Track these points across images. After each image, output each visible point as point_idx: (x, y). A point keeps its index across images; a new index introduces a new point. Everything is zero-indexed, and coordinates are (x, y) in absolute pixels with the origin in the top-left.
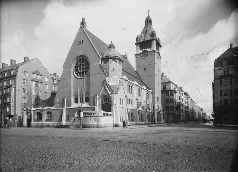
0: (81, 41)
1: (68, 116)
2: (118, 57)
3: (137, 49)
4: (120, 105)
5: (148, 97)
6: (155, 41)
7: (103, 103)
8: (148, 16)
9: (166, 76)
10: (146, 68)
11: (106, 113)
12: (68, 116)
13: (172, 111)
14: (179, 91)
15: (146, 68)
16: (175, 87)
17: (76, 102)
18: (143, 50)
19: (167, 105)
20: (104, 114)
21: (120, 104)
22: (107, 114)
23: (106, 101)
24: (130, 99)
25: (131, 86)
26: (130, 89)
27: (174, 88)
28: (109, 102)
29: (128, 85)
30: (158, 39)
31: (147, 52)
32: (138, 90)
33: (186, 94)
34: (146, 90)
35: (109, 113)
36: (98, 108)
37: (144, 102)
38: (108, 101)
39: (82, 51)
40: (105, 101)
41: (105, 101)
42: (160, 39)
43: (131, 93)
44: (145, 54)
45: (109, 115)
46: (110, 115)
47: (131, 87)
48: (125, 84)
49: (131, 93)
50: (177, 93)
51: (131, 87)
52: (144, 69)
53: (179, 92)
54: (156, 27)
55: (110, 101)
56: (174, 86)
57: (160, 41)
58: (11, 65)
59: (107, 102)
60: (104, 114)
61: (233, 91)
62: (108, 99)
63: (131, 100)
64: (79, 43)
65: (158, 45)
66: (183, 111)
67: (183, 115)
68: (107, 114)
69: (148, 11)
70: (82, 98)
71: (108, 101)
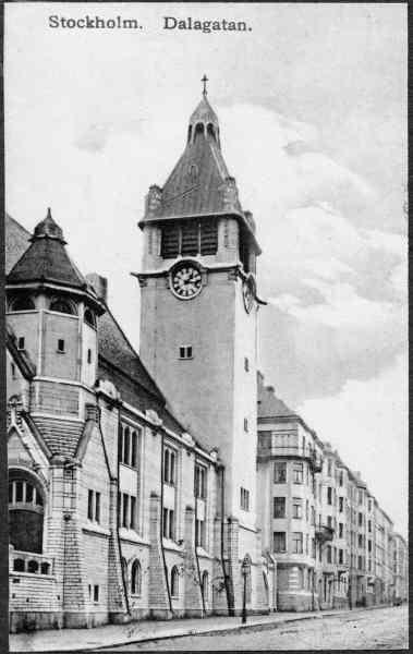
4: (88, 521)
5: (200, 493)
6: (233, 226)
8: (205, 104)
10: (190, 350)
13: (284, 556)
16: (312, 442)
18: (175, 261)
19: (280, 525)
21: (90, 517)
26: (128, 453)
28: (34, 506)
29: (167, 452)
30: (248, 214)
32: (120, 428)
34: (197, 453)
37: (184, 507)
38: (29, 499)
42: (256, 217)
43: (133, 464)
47: (173, 456)
48: (110, 420)
49: (133, 464)
50: (319, 470)
51: (173, 456)
54: (237, 154)
55: (40, 501)
56: (309, 438)
57: (253, 225)
60: (19, 565)
61: (194, 127)
63: (133, 498)
65: (247, 246)
67: (343, 575)
69: (205, 79)
71: (29, 499)
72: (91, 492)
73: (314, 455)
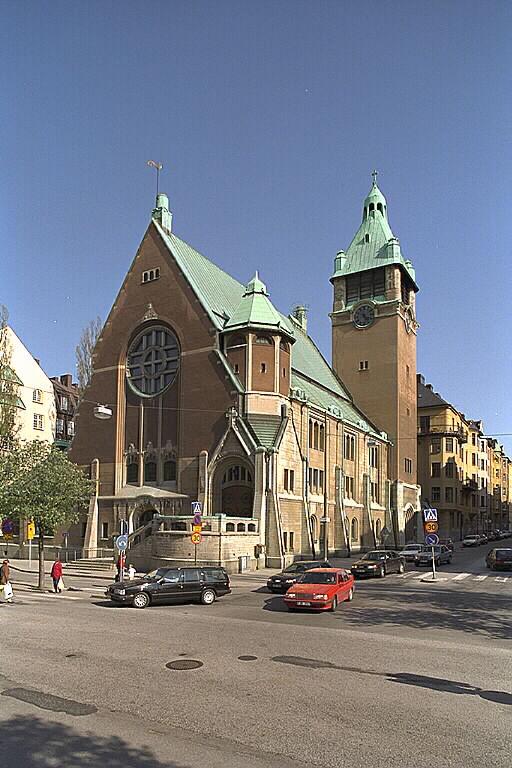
1: (105, 527)
2: (277, 325)
3: (337, 299)
5: (375, 463)
6: (397, 272)
7: (226, 485)
9: (429, 386)
10: (366, 362)
11: (236, 520)
12: (106, 525)
14: (474, 435)
15: (366, 362)
17: (132, 478)
20: (230, 527)
22: (241, 527)
24: (315, 470)
27: (456, 424)
31: (372, 309)
32: (310, 422)
33: (492, 443)
35: (246, 521)
36: (204, 505)
39: (153, 306)
44: (366, 317)
45: (247, 529)
46: (251, 527)
51: (352, 439)
52: (362, 363)
53: (474, 440)
56: (458, 419)
59: (240, 482)
60: (230, 527)
62: (243, 470)
63: (321, 471)
70: (288, 535)
72: (286, 470)
73: (462, 431)
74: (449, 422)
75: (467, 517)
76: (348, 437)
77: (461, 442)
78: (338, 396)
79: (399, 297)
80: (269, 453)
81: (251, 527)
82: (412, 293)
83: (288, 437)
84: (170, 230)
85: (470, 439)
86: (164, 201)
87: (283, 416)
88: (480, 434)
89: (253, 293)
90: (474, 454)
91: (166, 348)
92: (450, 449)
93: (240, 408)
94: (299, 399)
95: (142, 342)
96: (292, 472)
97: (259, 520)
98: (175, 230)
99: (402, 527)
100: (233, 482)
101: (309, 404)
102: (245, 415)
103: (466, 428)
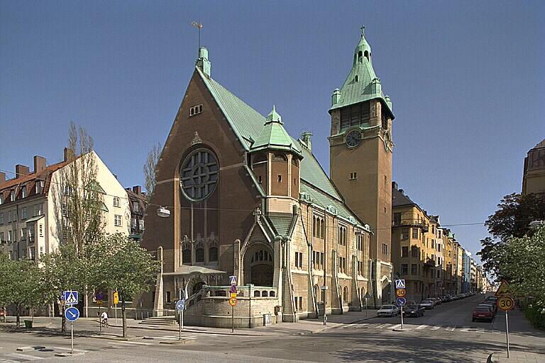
0: (197, 108)
2: (290, 146)
6: (379, 104)
7: (253, 264)
9: (401, 191)
10: (355, 173)
11: (261, 289)
12: (169, 293)
20: (257, 293)
21: (296, 265)
22: (265, 294)
23: (261, 259)
25: (321, 219)
28: (268, 262)
35: (269, 289)
36: (238, 278)
39: (199, 134)
40: (257, 259)
41: (257, 259)
44: (355, 140)
46: (272, 294)
47: (344, 230)
49: (322, 236)
51: (344, 230)
52: (352, 174)
53: (433, 229)
58: (35, 169)
59: (264, 262)
60: (257, 293)
64: (352, 177)
66: (438, 274)
68: (263, 292)
72: (297, 253)
73: (425, 224)
74: (415, 217)
75: (426, 285)
76: (318, 219)
77: (423, 231)
78: (334, 199)
79: (380, 124)
80: (285, 241)
81: (272, 294)
82: (389, 121)
83: (297, 229)
84: (209, 75)
85: (430, 229)
86: (205, 53)
87: (294, 214)
88: (438, 225)
89: (272, 122)
90: (433, 240)
91: (209, 164)
92: (415, 237)
93: (263, 208)
94: (306, 201)
95: (191, 160)
96: (301, 254)
97: (278, 288)
98: (213, 76)
99: (380, 293)
100: (259, 262)
101: (313, 204)
102: (267, 213)
103: (427, 221)
